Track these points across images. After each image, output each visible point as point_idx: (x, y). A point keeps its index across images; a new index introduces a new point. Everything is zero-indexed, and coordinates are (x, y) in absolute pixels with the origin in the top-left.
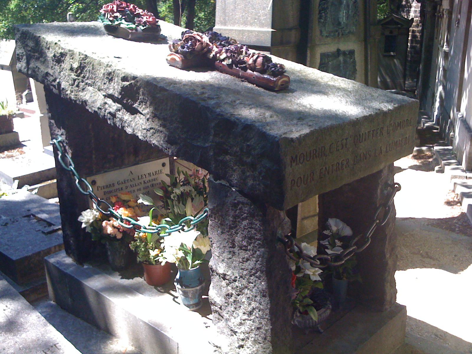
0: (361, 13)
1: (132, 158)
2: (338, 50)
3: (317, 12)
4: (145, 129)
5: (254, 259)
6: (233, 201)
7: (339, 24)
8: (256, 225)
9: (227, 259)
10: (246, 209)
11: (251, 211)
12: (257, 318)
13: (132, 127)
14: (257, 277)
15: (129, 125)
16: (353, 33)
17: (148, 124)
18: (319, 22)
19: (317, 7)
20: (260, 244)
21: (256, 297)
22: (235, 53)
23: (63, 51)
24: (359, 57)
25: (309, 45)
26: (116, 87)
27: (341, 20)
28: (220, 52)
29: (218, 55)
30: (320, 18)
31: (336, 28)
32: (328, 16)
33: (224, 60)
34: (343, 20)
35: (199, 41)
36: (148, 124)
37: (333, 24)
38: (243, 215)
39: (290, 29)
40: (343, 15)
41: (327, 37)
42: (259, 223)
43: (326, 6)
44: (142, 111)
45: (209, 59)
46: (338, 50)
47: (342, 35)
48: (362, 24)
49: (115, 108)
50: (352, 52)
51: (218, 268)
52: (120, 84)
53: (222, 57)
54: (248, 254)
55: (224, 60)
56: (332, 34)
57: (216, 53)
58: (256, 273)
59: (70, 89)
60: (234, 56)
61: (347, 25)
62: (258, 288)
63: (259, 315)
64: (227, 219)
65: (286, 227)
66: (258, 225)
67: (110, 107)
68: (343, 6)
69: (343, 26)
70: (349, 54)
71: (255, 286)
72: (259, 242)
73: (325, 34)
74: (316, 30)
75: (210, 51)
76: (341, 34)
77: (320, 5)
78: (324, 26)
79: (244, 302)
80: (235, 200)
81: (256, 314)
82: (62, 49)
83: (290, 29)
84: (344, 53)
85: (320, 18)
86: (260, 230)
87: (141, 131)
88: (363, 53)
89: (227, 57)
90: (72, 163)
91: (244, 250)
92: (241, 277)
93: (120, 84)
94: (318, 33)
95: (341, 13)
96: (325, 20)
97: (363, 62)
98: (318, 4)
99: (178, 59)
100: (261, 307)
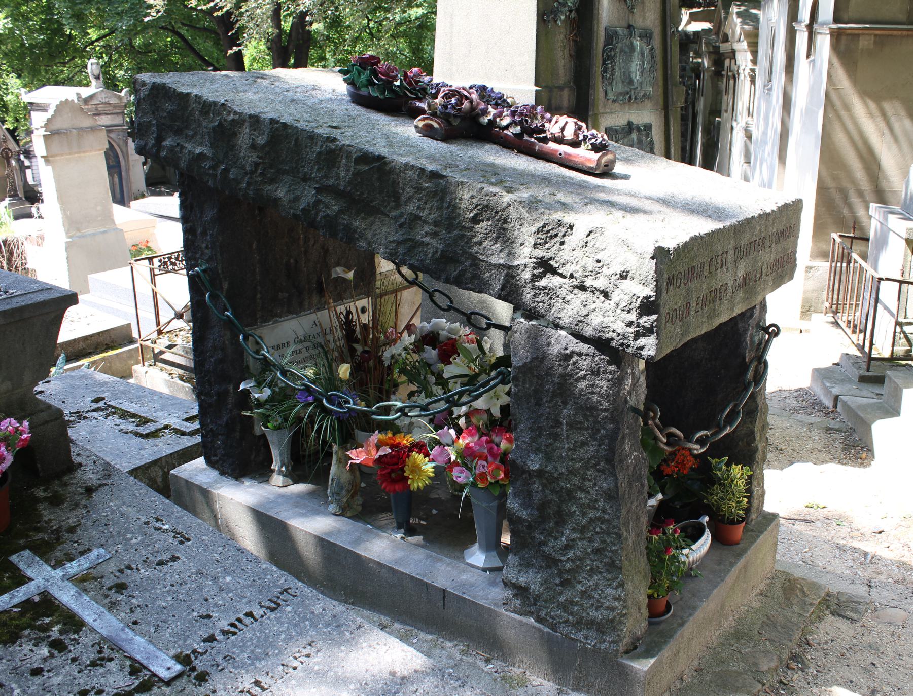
0: (659, 66)
1: (315, 299)
2: (630, 124)
3: (601, 62)
4: (393, 242)
5: (596, 443)
6: (563, 352)
7: (631, 82)
8: (602, 387)
9: (546, 446)
10: (585, 363)
11: (594, 365)
12: (597, 533)
13: (366, 239)
14: (599, 471)
15: (361, 237)
16: (649, 97)
17: (400, 232)
18: (603, 77)
19: (600, 55)
20: (606, 417)
21: (596, 501)
22: (526, 116)
23: (236, 117)
24: (657, 135)
25: (591, 113)
26: (343, 174)
27: (633, 76)
28: (500, 115)
29: (498, 120)
30: (605, 71)
31: (626, 89)
32: (617, 68)
33: (507, 127)
34: (636, 76)
35: (467, 98)
36: (400, 232)
37: (623, 82)
38: (577, 373)
39: (561, 88)
40: (635, 67)
41: (614, 101)
42: (607, 384)
43: (613, 53)
44: (389, 211)
45: (481, 125)
46: (630, 124)
47: (635, 99)
48: (661, 83)
49: (336, 208)
50: (648, 127)
51: (529, 463)
52: (352, 169)
53: (505, 122)
54: (583, 435)
55: (507, 127)
56: (621, 98)
57: (495, 117)
58: (599, 464)
59: (246, 179)
60: (526, 121)
61: (641, 83)
62: (600, 487)
63: (601, 529)
64: (548, 381)
65: (640, 392)
66: (605, 387)
67: (327, 207)
68: (636, 54)
69: (636, 85)
70: (645, 130)
71: (595, 484)
72: (606, 414)
73: (611, 96)
74: (599, 89)
75: (485, 112)
76: (633, 97)
77: (604, 51)
78: (611, 84)
79: (574, 512)
80: (566, 349)
81: (595, 529)
82: (235, 113)
83: (561, 88)
84: (638, 128)
85: (605, 71)
86: (608, 396)
87: (384, 245)
88: (663, 128)
89: (513, 123)
90: (228, 306)
91: (577, 429)
92: (570, 472)
93: (352, 169)
94: (601, 94)
95: (633, 65)
96: (612, 75)
97: (663, 143)
98: (601, 50)
99: (436, 125)
100: (606, 517)
